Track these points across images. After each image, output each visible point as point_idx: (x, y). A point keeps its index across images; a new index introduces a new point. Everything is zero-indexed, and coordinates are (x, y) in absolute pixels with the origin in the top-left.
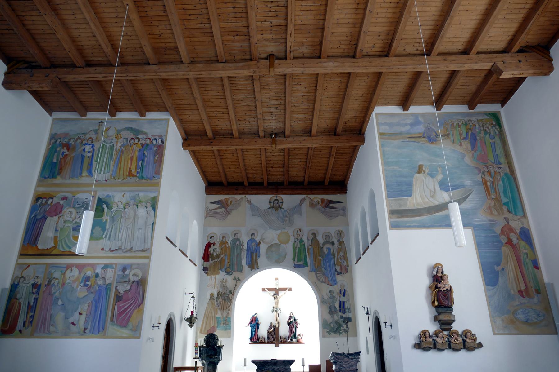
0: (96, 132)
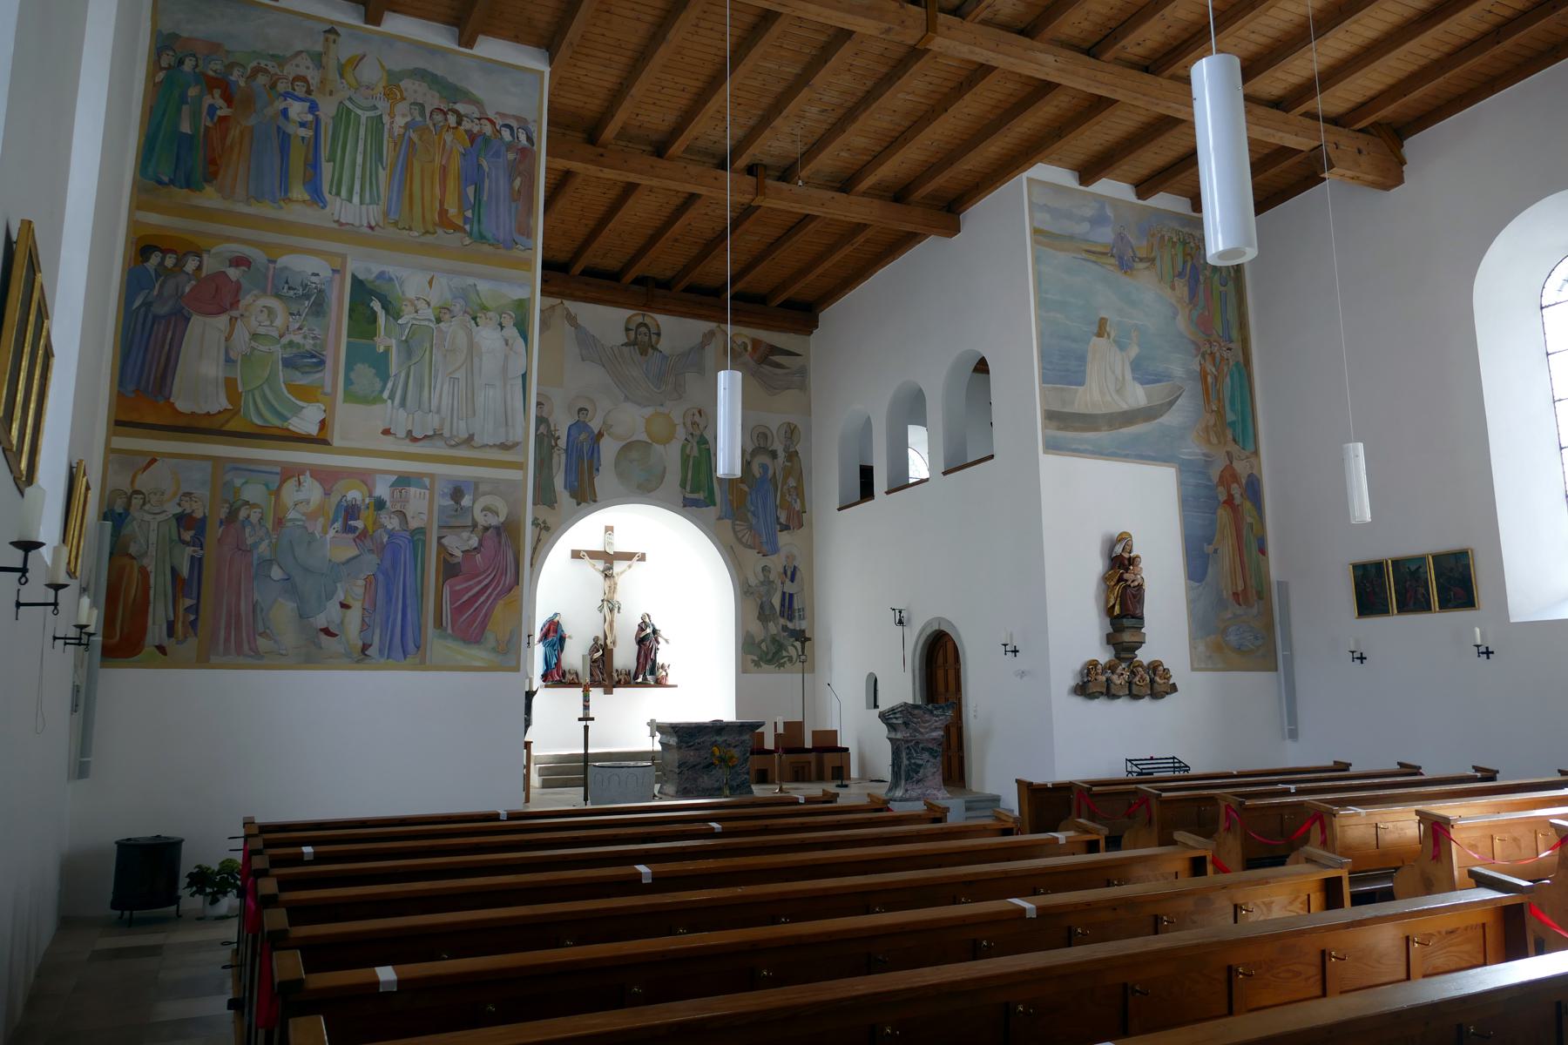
0: (318, 60)
